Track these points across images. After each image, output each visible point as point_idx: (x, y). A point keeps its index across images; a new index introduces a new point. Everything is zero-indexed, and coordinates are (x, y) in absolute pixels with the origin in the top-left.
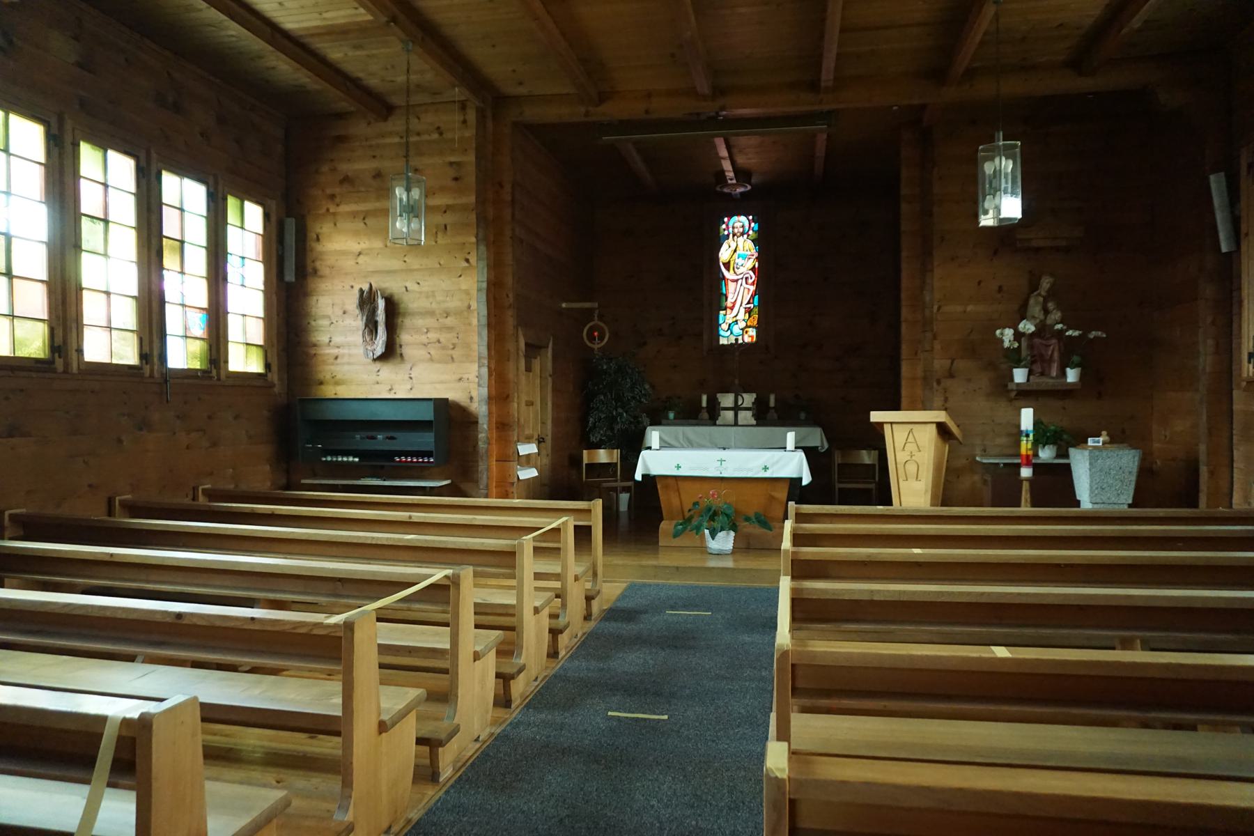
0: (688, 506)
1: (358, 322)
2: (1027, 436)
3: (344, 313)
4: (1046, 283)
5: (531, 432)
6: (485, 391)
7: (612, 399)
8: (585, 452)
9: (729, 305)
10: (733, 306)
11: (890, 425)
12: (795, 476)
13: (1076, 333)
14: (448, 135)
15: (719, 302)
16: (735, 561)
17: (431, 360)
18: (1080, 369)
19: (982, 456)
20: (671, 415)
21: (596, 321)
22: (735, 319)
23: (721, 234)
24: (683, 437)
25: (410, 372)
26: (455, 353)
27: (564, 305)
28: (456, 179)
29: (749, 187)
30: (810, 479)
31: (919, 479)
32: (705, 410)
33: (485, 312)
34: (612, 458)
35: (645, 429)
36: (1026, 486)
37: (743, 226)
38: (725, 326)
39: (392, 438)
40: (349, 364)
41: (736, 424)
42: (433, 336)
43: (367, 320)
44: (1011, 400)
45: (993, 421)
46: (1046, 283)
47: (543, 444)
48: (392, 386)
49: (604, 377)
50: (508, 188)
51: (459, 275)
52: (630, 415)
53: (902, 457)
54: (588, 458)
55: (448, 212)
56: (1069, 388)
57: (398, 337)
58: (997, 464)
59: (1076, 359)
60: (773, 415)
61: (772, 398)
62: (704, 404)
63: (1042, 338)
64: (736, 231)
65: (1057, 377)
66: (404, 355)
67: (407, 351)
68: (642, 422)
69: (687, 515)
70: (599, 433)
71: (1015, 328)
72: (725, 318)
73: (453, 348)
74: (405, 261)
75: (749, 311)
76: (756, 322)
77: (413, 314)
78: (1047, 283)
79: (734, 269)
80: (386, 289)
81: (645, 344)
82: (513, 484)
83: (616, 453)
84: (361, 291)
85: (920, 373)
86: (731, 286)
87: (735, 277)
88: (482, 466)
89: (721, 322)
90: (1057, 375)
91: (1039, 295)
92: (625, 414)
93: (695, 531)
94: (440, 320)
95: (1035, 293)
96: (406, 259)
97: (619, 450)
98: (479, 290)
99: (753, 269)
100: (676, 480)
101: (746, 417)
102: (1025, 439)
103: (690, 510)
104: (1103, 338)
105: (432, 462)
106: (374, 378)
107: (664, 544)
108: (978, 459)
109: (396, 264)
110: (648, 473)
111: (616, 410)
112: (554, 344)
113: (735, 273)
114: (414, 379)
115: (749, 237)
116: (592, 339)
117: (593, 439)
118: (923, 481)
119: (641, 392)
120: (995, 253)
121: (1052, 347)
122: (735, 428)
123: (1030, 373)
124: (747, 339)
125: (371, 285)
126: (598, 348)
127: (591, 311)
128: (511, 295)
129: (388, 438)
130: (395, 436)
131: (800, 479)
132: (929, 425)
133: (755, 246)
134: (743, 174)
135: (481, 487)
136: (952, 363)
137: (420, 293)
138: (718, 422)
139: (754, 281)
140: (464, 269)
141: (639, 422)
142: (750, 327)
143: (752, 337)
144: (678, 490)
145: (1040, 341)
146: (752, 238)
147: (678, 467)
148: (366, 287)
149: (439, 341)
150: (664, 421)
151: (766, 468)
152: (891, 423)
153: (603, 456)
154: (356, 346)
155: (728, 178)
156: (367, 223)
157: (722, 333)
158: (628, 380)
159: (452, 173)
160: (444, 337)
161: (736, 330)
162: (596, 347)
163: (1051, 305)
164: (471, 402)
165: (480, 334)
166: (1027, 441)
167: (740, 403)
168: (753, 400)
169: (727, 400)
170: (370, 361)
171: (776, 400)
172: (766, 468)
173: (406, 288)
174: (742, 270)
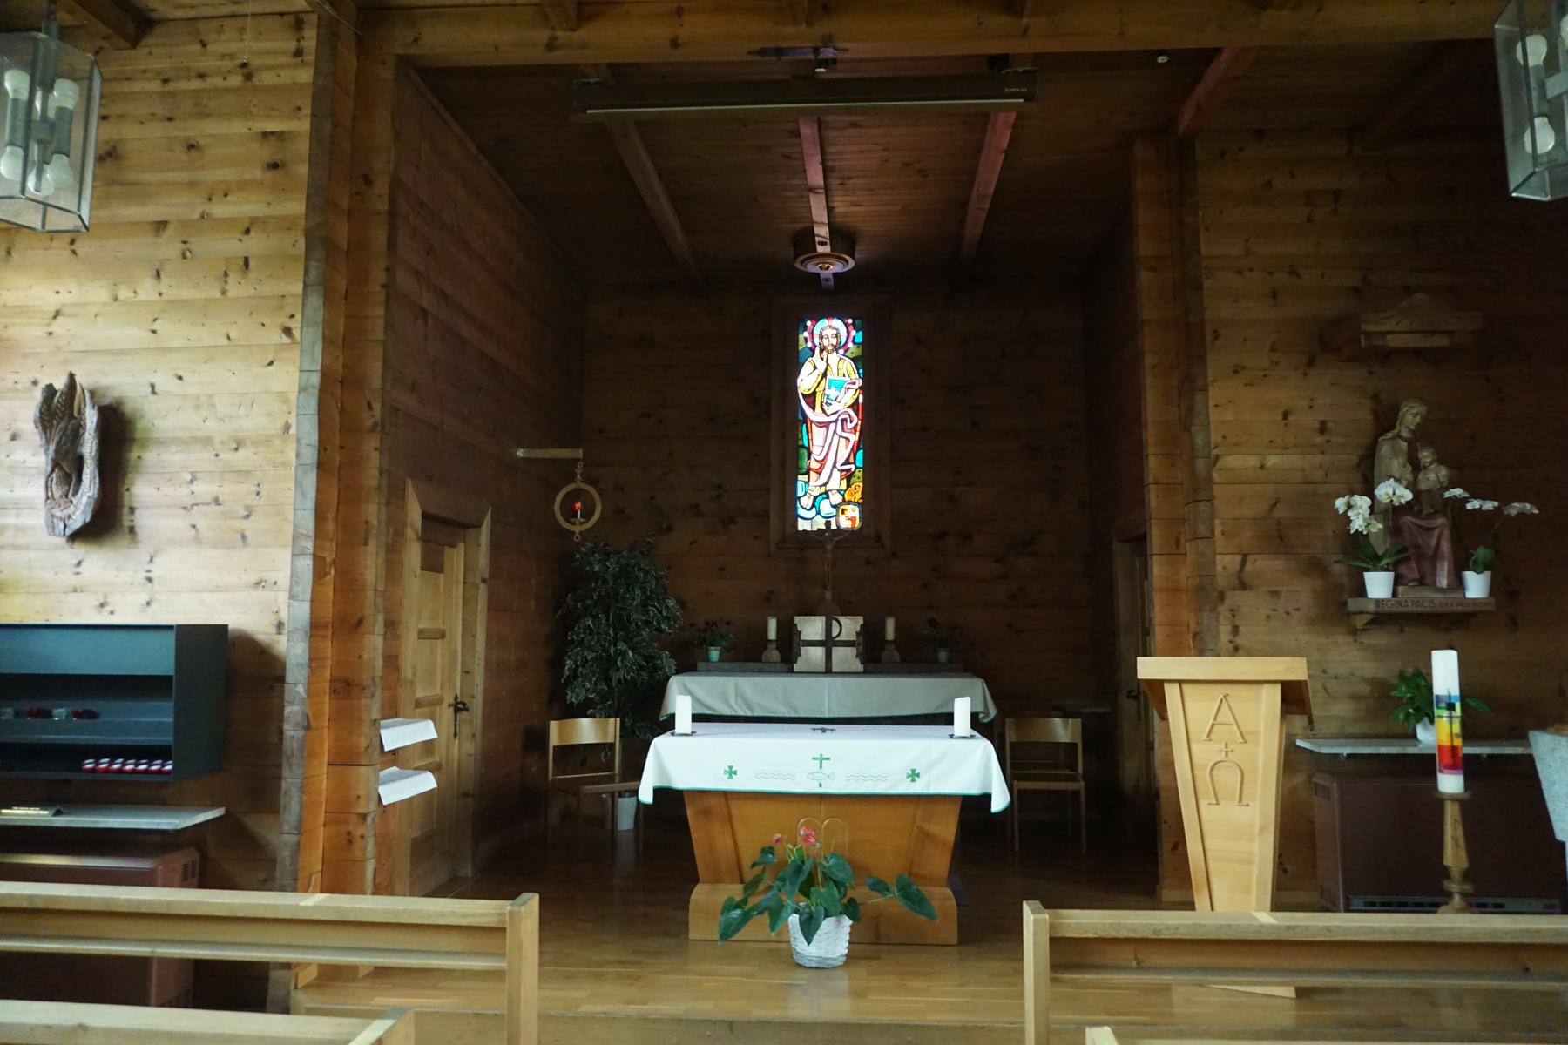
0: (749, 854)
1: (35, 456)
2: (1451, 707)
3: (14, 437)
4: (1411, 415)
5: (439, 693)
6: (303, 610)
7: (609, 626)
8: (554, 725)
9: (814, 465)
10: (822, 467)
11: (1177, 686)
12: (975, 791)
13: (1489, 505)
14: (266, 78)
15: (797, 457)
16: (857, 994)
17: (198, 541)
18: (1488, 574)
19: (1306, 738)
20: (714, 654)
21: (579, 484)
22: (823, 490)
23: (800, 348)
24: (737, 695)
25: (150, 567)
26: (249, 526)
27: (520, 453)
28: (274, 166)
29: (852, 264)
30: (1008, 799)
31: (1244, 802)
32: (774, 646)
33: (314, 438)
34: (605, 733)
35: (668, 679)
36: (1451, 814)
37: (837, 335)
38: (806, 501)
39: (92, 715)
40: (15, 547)
41: (828, 671)
42: (204, 489)
43: (56, 452)
44: (1354, 632)
45: (1324, 671)
46: (1411, 415)
47: (463, 715)
48: (105, 597)
49: (593, 585)
50: (382, 186)
51: (269, 361)
52: (640, 654)
53: (1205, 753)
54: (561, 736)
55: (252, 233)
56: (1471, 608)
57: (128, 490)
58: (1337, 755)
59: (1482, 553)
60: (891, 654)
61: (890, 625)
62: (772, 635)
63: (1417, 514)
64: (825, 342)
65: (1450, 588)
66: (137, 529)
67: (144, 520)
68: (662, 668)
69: (749, 875)
70: (584, 686)
71: (1372, 496)
72: (807, 489)
73: (248, 516)
74: (154, 332)
75: (848, 476)
76: (858, 495)
77: (162, 443)
78: (1416, 415)
79: (822, 405)
80: (107, 388)
81: (669, 529)
82: (363, 817)
83: (613, 724)
84: (50, 391)
85: (1186, 576)
86: (818, 435)
87: (824, 419)
88: (290, 780)
89: (800, 493)
90: (1449, 584)
91: (1399, 436)
92: (630, 653)
93: (557, 43)
94: (223, 456)
95: (1390, 435)
96: (156, 326)
97: (618, 719)
98: (302, 390)
99: (854, 406)
100: (727, 799)
101: (845, 657)
102: (1445, 713)
103: (754, 865)
104: (1534, 514)
105: (169, 772)
106: (68, 578)
107: (698, 937)
108: (1299, 743)
109: (132, 334)
110: (665, 784)
111: (615, 646)
112: (494, 522)
113: (824, 411)
114: (155, 582)
115: (848, 354)
116: (570, 514)
117: (571, 697)
118: (1256, 806)
119: (661, 612)
120: (1311, 362)
121: (1436, 533)
122: (827, 680)
123: (1397, 581)
124: (845, 524)
125: (72, 377)
126: (581, 533)
127: (573, 462)
128: (377, 406)
129: (77, 714)
130: (94, 709)
131: (986, 798)
132: (1266, 687)
133: (858, 369)
134: (844, 238)
135: (286, 828)
136: (1243, 563)
137: (184, 397)
138: (797, 667)
139: (857, 425)
140: (281, 348)
141: (656, 668)
142: (849, 502)
143: (853, 519)
144: (730, 819)
145: (1413, 520)
146: (852, 356)
147: (731, 772)
148: (60, 384)
149: (217, 501)
150: (701, 665)
151: (914, 775)
152: (1180, 682)
153: (587, 731)
154: (32, 507)
155: (817, 239)
156: (78, 251)
157: (801, 512)
158: (638, 592)
159: (266, 152)
160: (227, 490)
161: (826, 507)
162: (577, 529)
163: (1426, 456)
164: (279, 633)
165: (298, 483)
166: (1451, 717)
167: (835, 632)
168: (858, 629)
169: (812, 628)
170: (63, 540)
171: (897, 627)
172: (914, 775)
173: (153, 386)
174: (835, 407)
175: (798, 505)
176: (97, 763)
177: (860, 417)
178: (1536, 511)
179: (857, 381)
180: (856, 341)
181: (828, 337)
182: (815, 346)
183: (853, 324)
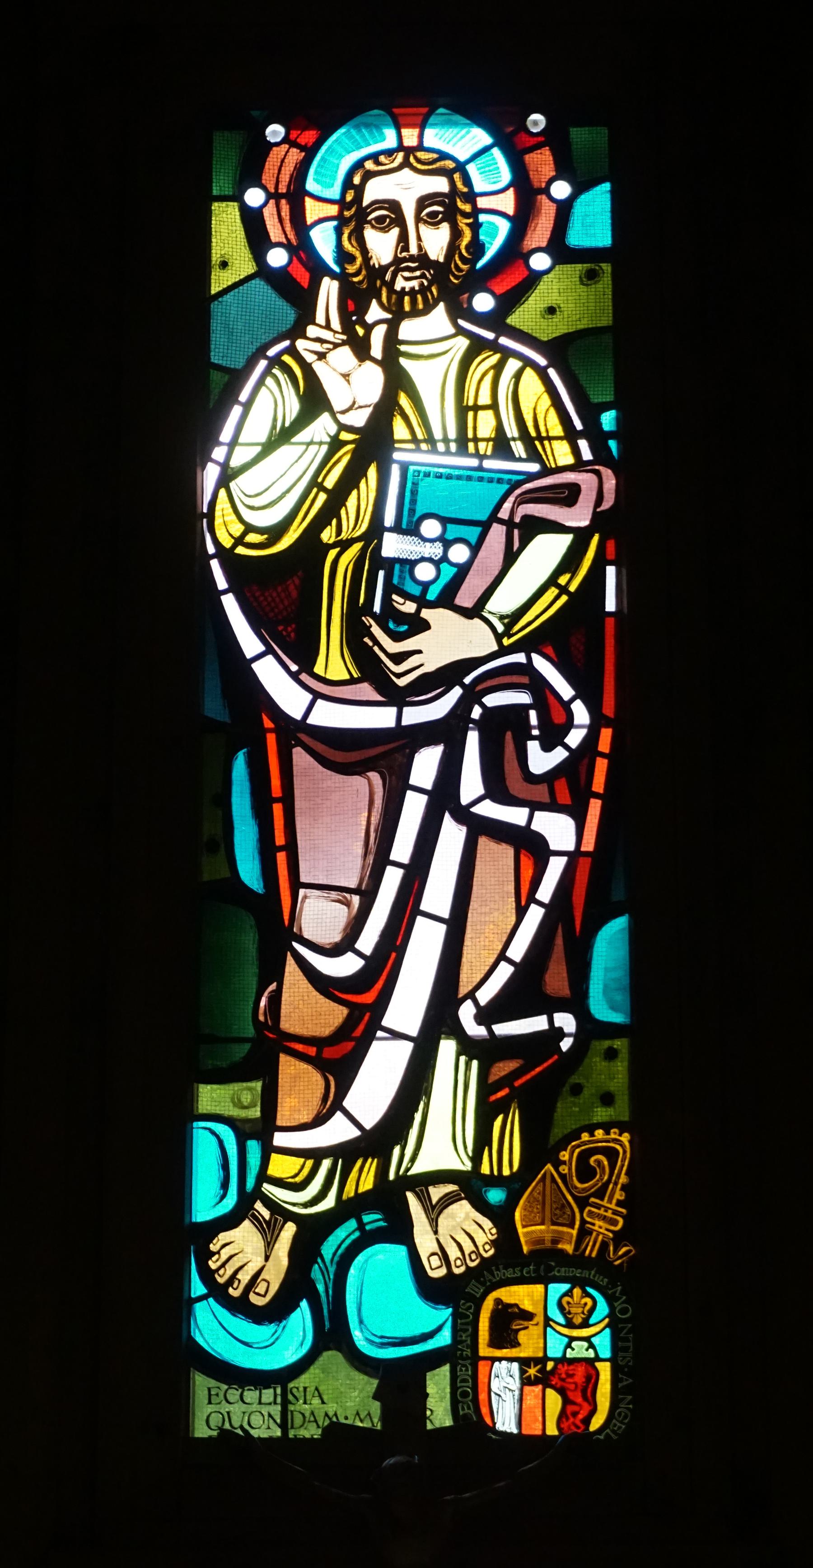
23: (219, 281)
175: (198, 1288)
176: (592, 1135)
177: (609, 709)
178: (509, 1310)
179: (586, 480)
180: (576, 237)
181: (399, 220)
182: (318, 270)
183: (548, 138)
